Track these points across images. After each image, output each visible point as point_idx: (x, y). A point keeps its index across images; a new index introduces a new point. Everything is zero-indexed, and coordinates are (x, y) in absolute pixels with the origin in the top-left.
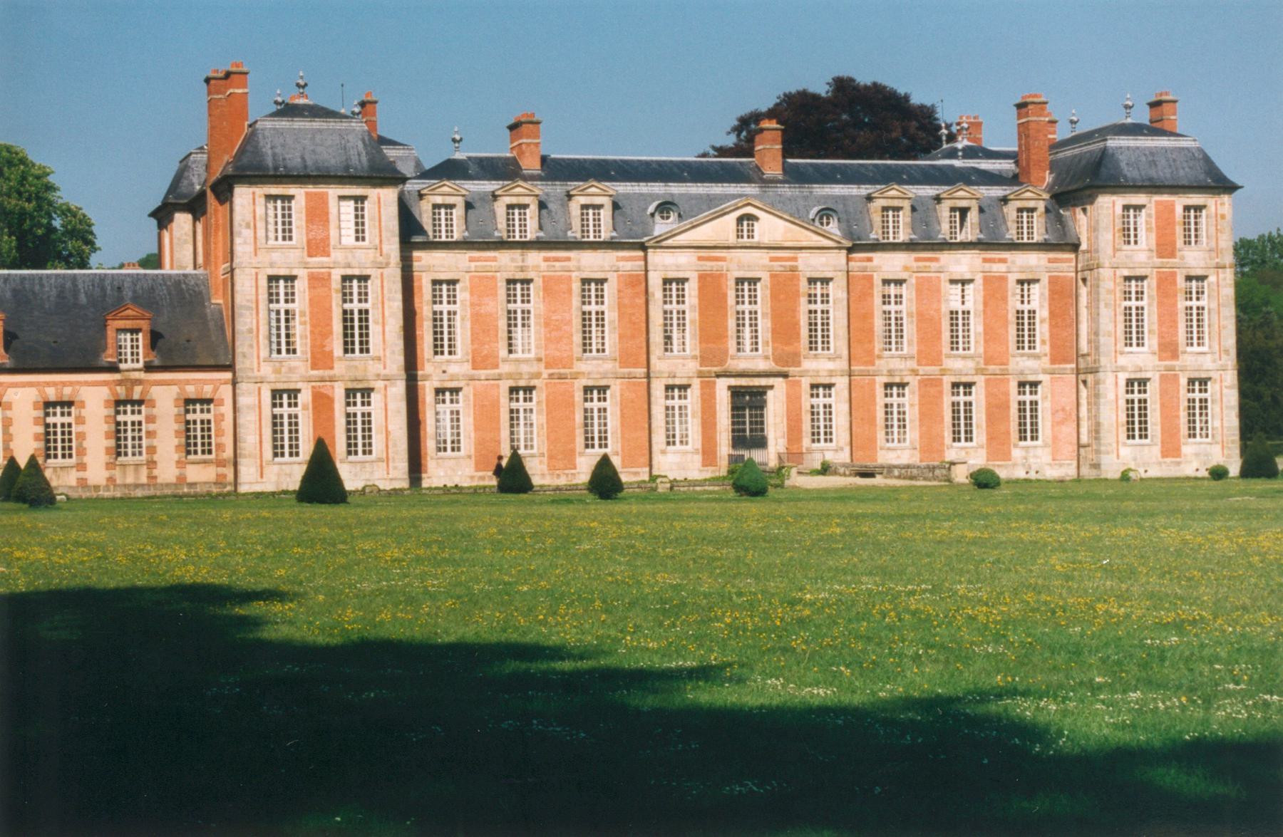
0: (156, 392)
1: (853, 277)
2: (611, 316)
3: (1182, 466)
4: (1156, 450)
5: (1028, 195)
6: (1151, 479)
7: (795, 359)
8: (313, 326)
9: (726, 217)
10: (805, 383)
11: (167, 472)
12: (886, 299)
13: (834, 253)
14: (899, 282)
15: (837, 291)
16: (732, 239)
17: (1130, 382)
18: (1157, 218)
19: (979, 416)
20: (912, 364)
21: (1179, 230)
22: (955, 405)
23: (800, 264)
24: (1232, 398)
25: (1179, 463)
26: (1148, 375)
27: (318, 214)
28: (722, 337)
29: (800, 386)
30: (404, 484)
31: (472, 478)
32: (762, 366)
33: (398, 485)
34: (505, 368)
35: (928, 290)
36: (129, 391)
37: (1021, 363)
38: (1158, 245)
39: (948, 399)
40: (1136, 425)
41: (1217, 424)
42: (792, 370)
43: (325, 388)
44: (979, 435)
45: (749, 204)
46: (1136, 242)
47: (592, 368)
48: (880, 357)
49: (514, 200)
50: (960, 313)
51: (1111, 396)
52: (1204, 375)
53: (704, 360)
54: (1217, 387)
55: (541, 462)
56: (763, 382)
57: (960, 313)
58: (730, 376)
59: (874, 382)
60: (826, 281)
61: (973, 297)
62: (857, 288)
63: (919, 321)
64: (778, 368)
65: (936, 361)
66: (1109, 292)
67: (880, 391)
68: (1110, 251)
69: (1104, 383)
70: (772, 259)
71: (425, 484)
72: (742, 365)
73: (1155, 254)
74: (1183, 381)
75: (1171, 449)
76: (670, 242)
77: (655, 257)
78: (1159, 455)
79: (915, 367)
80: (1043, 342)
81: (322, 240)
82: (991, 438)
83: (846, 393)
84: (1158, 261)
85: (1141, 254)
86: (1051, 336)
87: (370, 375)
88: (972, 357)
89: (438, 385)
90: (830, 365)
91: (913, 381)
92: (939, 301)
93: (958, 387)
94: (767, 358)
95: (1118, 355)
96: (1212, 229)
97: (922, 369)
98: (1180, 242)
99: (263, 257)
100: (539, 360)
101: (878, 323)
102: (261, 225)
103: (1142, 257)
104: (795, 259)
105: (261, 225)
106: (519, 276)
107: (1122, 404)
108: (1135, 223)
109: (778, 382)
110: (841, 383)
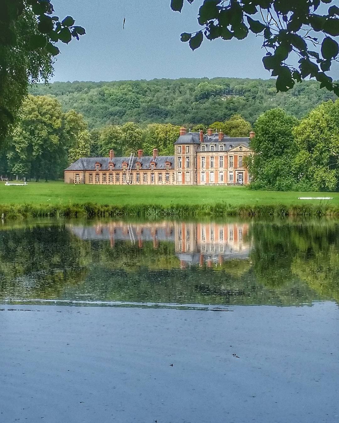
53: (234, 168)
72: (239, 169)
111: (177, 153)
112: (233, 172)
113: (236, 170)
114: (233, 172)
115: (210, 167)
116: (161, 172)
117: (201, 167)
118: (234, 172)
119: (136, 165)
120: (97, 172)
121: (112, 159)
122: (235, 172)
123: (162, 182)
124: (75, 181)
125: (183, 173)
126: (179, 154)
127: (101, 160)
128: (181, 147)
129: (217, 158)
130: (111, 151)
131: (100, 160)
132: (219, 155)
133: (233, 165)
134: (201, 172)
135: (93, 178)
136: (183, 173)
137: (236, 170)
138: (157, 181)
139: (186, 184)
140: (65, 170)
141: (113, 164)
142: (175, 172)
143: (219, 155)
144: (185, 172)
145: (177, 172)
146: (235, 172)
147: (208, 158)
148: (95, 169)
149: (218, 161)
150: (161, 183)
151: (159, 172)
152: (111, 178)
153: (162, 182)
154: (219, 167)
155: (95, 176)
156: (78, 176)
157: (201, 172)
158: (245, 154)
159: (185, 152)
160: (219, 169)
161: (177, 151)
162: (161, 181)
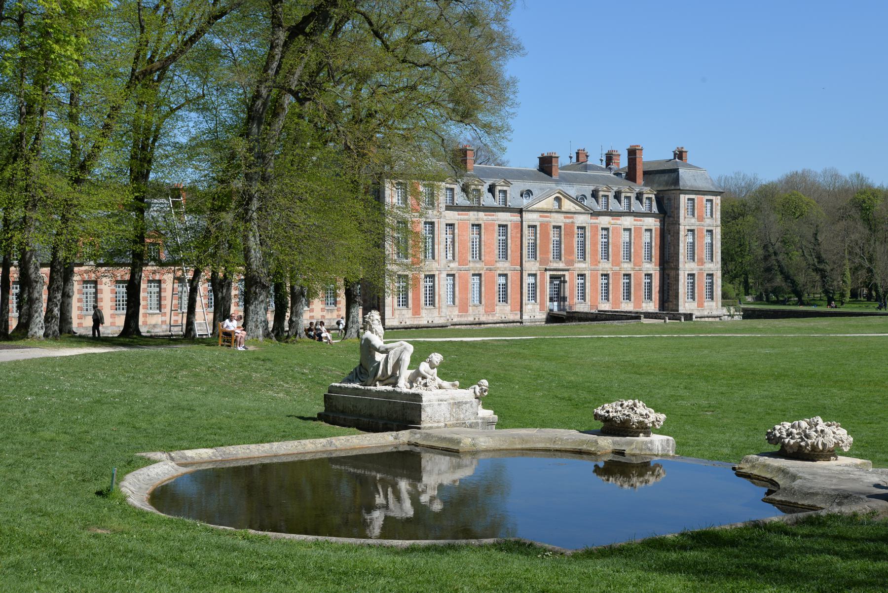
58: (550, 270)
109: (566, 273)
113: (546, 270)
122: (542, 275)
146: (542, 275)
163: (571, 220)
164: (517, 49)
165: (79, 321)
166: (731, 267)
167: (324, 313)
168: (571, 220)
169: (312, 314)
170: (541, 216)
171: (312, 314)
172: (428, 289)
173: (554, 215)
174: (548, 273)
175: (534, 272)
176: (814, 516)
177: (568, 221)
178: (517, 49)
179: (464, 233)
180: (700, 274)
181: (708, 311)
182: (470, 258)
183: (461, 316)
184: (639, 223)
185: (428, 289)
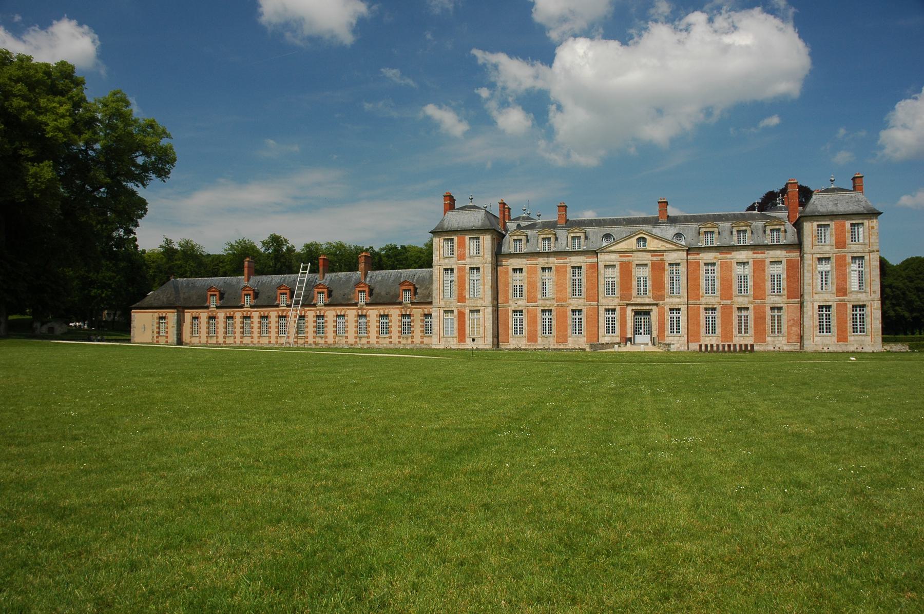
0: (219, 315)
1: (690, 262)
2: (584, 281)
3: (848, 346)
4: (835, 339)
5: (742, 224)
6: (865, 353)
7: (662, 298)
8: (459, 286)
9: (632, 239)
10: (667, 308)
11: (330, 340)
12: (707, 271)
13: (680, 253)
14: (714, 264)
15: (683, 269)
16: (634, 248)
17: (820, 307)
18: (836, 230)
19: (751, 323)
20: (718, 300)
21: (848, 235)
22: (773, 317)
23: (665, 258)
24: (878, 314)
25: (846, 345)
26: (830, 303)
27: (462, 245)
28: (630, 288)
29: (732, 308)
30: (489, 346)
31: (526, 345)
32: (647, 301)
33: (487, 347)
34: (540, 302)
35: (726, 267)
36: (320, 312)
37: (772, 299)
38: (836, 242)
39: (735, 314)
40: (824, 326)
41: (869, 327)
42: (661, 302)
43: (462, 309)
44: (751, 331)
45: (641, 233)
46: (825, 242)
47: (575, 303)
48: (702, 297)
49: (545, 236)
50: (776, 276)
51: (810, 313)
52: (861, 303)
53: (622, 298)
54: (869, 308)
55: (553, 340)
56: (651, 307)
57: (776, 276)
58: (632, 305)
59: (699, 307)
60: (678, 264)
61: (748, 270)
62: (692, 268)
63: (721, 281)
64: (655, 302)
65: (730, 298)
66: (809, 265)
67: (511, 313)
68: (810, 246)
69: (807, 307)
70: (652, 256)
71: (503, 346)
72: (639, 301)
73: (834, 247)
74: (850, 306)
75: (842, 338)
76: (608, 250)
77: (601, 257)
78: (836, 341)
79: (720, 301)
80: (784, 289)
81: (463, 254)
82: (756, 333)
83: (686, 312)
84: (836, 250)
85: (828, 247)
86: (788, 286)
87: (479, 305)
88: (747, 296)
89: (513, 309)
90: (678, 300)
91: (751, 307)
92: (731, 272)
93: (823, 308)
94: (649, 297)
95: (814, 295)
96: (867, 234)
97: (723, 302)
98: (849, 241)
99: (816, 249)
100: (554, 299)
101: (702, 283)
102: (442, 250)
103: (827, 248)
104: (663, 255)
105: (442, 250)
106: (546, 266)
107: (816, 316)
108: (858, 232)
109: (654, 308)
110: (684, 308)
111: (442, 256)
112: (618, 308)
113: (627, 305)
114: (618, 308)
115: (539, 296)
116: (322, 312)
117: (510, 297)
118: (621, 309)
119: (278, 295)
120: (210, 311)
121: (248, 280)
122: (623, 311)
123: (390, 337)
124: (155, 332)
125: (461, 315)
126: (446, 260)
127: (221, 283)
128: (452, 240)
129: (560, 270)
130: (248, 261)
131: (219, 283)
132: (570, 262)
133: (584, 290)
134: (510, 310)
135: (201, 325)
136: (461, 315)
137: (627, 305)
138: (311, 334)
139: (468, 344)
140: (133, 306)
141: (219, 291)
142: (434, 309)
143: (570, 262)
144: (467, 311)
145: (442, 312)
146: (623, 311)
147: (532, 271)
148: (206, 305)
149: (566, 280)
150: (388, 340)
151: (245, 313)
152: (246, 326)
153: (390, 337)
154: (569, 295)
155: (207, 320)
156: (163, 321)
157: (510, 310)
158: (655, 258)
159: (467, 255)
160: (570, 301)
161: (442, 253)
162: (387, 335)
163: (659, 258)
164: (550, 29)
165: (241, 340)
166: (335, 270)
167: (401, 340)
168: (659, 258)
169: (391, 340)
170: (620, 256)
171: (391, 340)
172: (429, 331)
173: (635, 254)
174: (629, 309)
175: (613, 307)
176: (480, 62)
177: (655, 258)
178: (550, 29)
179: (533, 275)
180: (842, 306)
181: (856, 346)
182: (539, 296)
183: (529, 345)
184: (760, 256)
185: (429, 331)
